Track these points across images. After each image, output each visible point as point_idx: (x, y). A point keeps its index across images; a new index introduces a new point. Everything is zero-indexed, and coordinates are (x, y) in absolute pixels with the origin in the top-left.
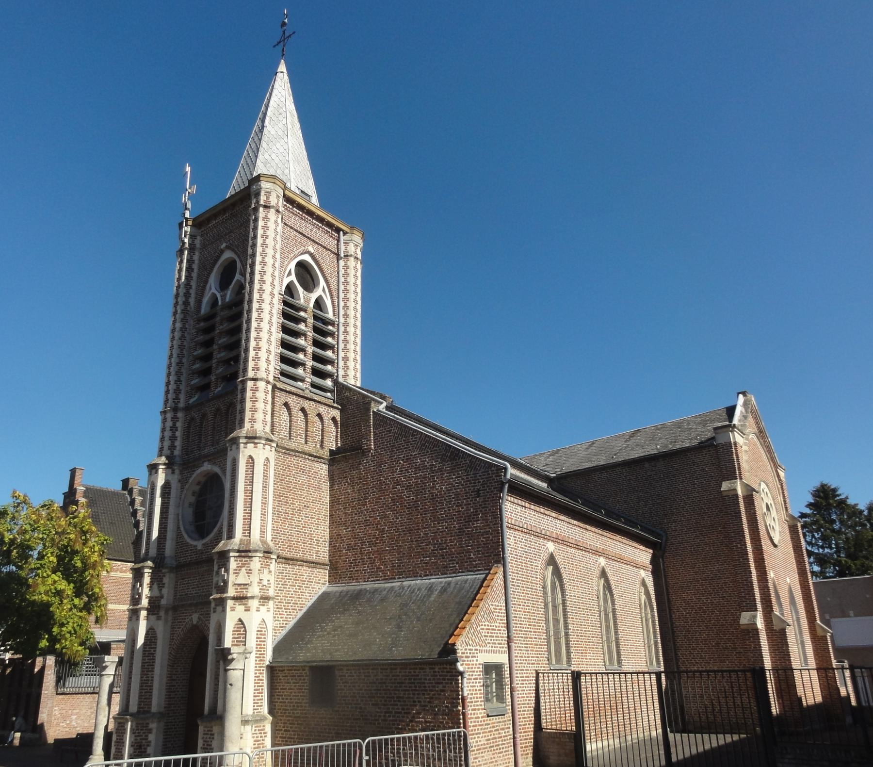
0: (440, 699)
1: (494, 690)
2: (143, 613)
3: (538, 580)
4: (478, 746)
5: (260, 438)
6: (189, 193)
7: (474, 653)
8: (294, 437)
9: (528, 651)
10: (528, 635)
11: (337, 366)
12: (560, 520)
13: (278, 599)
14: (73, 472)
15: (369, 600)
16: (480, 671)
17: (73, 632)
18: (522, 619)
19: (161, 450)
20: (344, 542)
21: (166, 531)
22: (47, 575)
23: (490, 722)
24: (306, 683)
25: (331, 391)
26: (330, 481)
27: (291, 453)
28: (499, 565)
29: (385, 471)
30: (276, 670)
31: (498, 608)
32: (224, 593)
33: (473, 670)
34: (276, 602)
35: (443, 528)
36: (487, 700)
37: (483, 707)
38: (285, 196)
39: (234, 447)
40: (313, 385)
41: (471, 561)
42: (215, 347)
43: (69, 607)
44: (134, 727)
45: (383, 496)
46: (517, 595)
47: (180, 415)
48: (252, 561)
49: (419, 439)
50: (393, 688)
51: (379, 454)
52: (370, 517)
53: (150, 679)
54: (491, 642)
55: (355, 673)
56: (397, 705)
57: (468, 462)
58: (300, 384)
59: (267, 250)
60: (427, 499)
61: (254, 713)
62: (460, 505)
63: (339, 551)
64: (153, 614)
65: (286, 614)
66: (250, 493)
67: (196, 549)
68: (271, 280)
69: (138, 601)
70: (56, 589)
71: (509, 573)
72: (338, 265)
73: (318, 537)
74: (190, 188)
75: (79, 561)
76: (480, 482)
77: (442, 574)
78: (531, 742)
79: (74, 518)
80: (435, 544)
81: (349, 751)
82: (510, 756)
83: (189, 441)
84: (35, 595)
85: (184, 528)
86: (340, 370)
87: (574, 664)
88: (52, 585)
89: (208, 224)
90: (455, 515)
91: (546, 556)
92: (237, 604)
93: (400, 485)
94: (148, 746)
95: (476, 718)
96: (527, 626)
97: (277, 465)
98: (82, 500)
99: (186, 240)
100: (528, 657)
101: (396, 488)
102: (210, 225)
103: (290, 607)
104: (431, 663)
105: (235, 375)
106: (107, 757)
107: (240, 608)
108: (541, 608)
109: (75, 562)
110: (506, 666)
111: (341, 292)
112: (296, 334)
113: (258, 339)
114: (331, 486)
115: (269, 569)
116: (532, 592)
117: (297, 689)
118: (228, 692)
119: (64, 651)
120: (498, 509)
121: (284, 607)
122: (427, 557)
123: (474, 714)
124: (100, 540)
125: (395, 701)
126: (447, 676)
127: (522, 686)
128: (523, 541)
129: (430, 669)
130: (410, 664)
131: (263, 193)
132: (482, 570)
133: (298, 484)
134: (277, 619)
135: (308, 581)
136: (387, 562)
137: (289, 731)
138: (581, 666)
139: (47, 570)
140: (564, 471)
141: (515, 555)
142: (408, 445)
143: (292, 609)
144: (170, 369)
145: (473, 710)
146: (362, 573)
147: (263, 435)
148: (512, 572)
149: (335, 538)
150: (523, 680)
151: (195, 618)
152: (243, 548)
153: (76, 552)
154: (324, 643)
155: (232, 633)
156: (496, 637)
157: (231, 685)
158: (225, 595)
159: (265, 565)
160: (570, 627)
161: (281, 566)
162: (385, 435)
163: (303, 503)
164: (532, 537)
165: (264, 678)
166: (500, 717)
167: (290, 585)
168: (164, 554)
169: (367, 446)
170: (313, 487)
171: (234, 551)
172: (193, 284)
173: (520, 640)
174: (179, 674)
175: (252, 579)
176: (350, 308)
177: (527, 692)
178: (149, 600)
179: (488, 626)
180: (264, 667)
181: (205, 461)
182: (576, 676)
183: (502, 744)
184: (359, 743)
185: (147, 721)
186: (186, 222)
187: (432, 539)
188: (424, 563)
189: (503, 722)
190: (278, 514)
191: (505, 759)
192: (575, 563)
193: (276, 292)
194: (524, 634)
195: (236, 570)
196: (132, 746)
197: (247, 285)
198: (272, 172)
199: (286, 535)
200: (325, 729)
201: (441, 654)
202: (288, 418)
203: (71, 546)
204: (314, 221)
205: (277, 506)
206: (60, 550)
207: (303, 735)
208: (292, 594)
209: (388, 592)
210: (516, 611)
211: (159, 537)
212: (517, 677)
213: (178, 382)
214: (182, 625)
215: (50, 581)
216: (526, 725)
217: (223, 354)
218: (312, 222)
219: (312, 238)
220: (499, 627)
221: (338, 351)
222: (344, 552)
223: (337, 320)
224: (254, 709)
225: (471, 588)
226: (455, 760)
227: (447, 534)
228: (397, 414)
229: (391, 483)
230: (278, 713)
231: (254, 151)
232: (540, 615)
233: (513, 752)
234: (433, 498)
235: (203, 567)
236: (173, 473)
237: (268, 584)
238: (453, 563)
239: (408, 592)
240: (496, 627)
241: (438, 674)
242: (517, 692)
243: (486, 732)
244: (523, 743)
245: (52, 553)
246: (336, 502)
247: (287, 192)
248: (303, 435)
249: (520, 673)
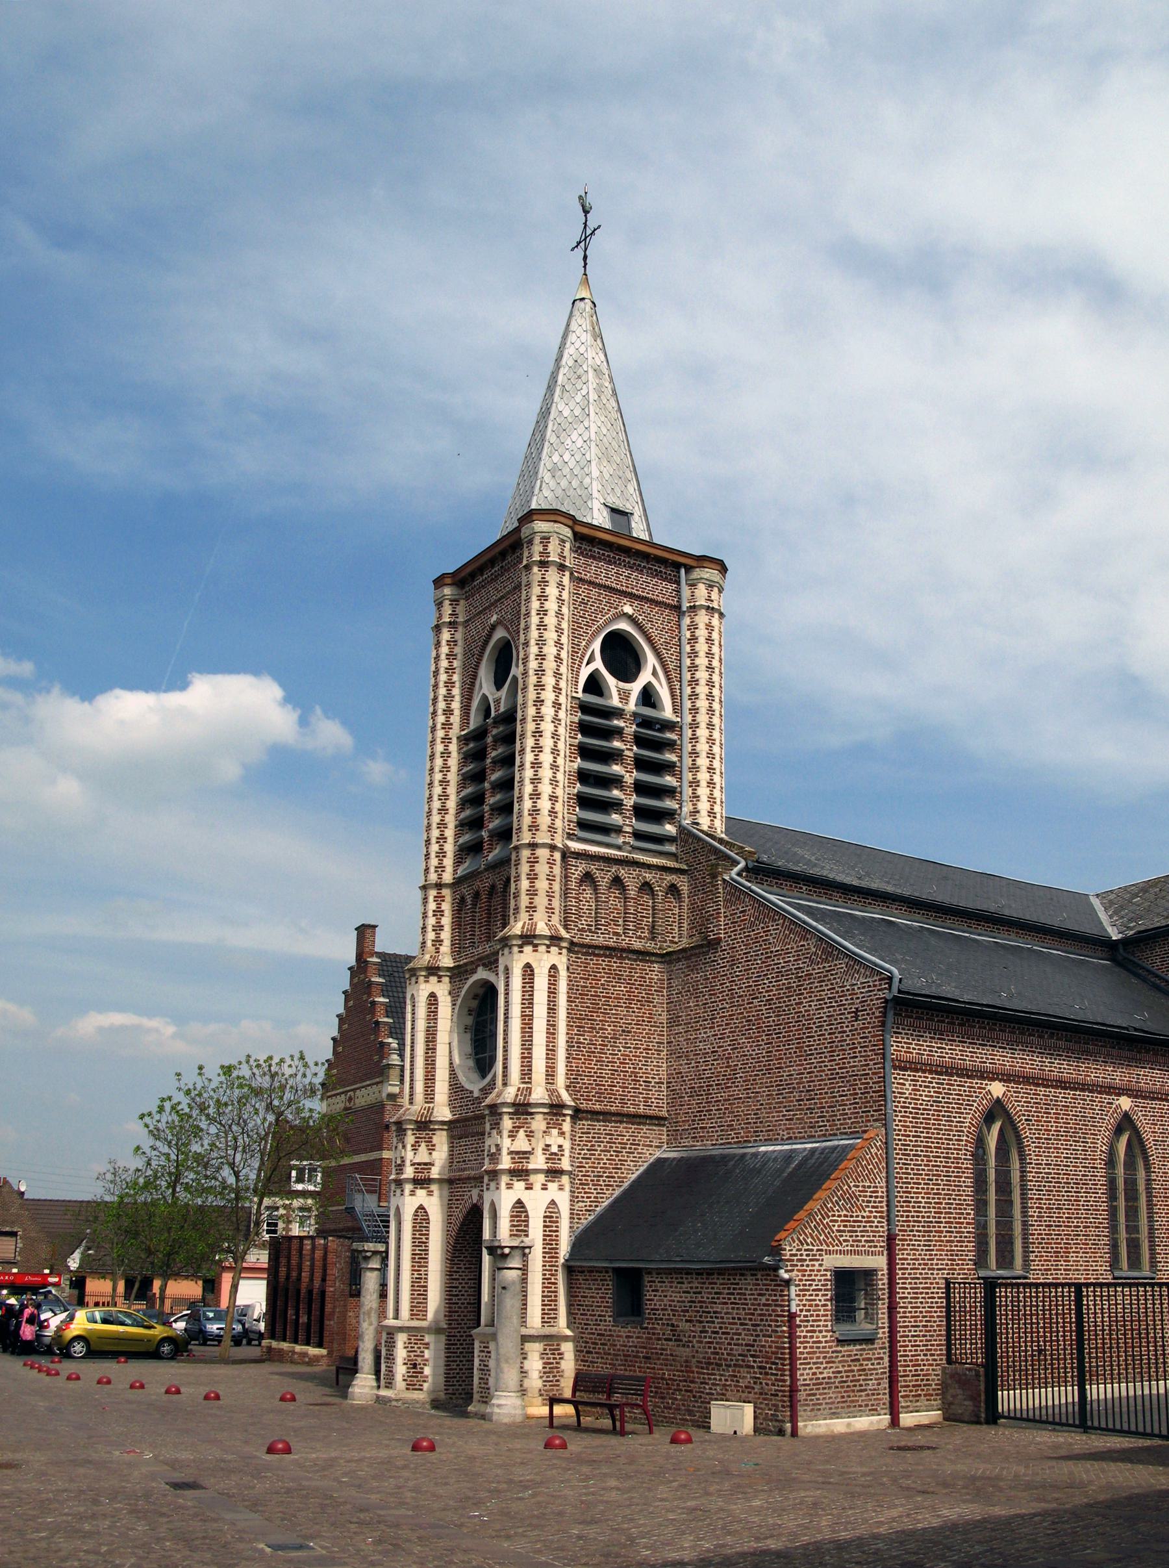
13: (581, 1171)
33: (813, 1277)
37: (830, 1328)
40: (638, 835)
47: (446, 892)
73: (647, 1077)
89: (473, 581)
103: (601, 1183)
107: (519, 1185)
115: (560, 1129)
131: (537, 540)
133: (610, 998)
137: (591, 1353)
143: (605, 1185)
159: (554, 1124)
170: (638, 1001)
181: (479, 966)
199: (593, 1076)
205: (576, 1034)
208: (605, 1164)
217: (498, 797)
247: (579, 529)
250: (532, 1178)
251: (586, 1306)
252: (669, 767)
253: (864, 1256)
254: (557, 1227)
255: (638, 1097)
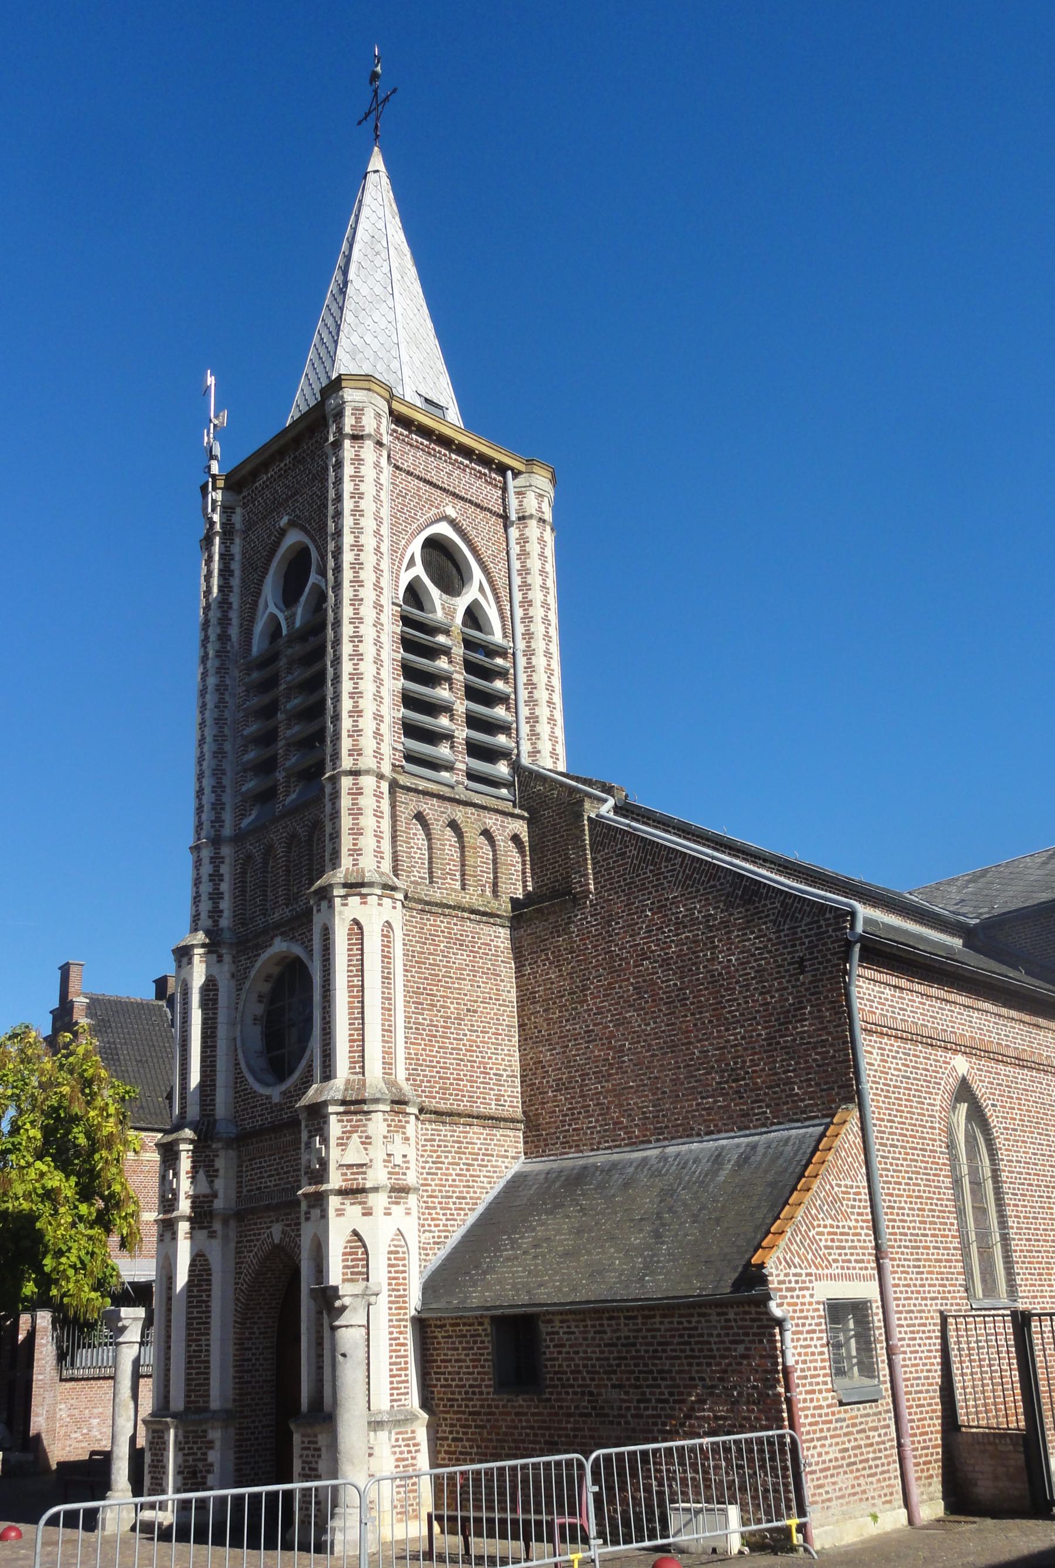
0: (740, 1372)
1: (854, 1353)
2: (184, 1227)
3: (937, 1131)
4: (824, 1462)
5: (371, 885)
6: (215, 426)
7: (804, 1282)
8: (438, 878)
9: (922, 1273)
10: (921, 1241)
11: (517, 735)
12: (978, 1010)
13: (427, 1191)
14: (65, 971)
15: (601, 1187)
16: (819, 1317)
17: (79, 1265)
18: (906, 1212)
19: (196, 918)
20: (549, 1076)
21: (215, 1071)
22: (27, 1162)
23: (847, 1416)
24: (487, 1348)
25: (509, 785)
26: (515, 958)
27: (434, 909)
28: (851, 1106)
29: (617, 934)
30: (430, 1326)
31: (852, 1191)
32: (321, 1182)
33: (805, 1314)
34: (422, 1197)
35: (736, 1039)
36: (839, 1372)
37: (830, 1386)
38: (391, 412)
39: (324, 904)
40: (472, 776)
41: (793, 1102)
42: (281, 716)
43: (69, 1219)
44: (181, 1438)
45: (616, 982)
46: (891, 1164)
47: (226, 851)
48: (370, 1120)
49: (681, 867)
50: (651, 1353)
51: (604, 902)
52: (594, 1025)
53: (204, 1348)
54: (840, 1258)
55: (577, 1327)
56: (659, 1386)
57: (777, 905)
58: (445, 775)
59: (363, 522)
60: (702, 984)
61: (392, 1406)
62: (768, 992)
63: (540, 1093)
64: (200, 1228)
65: (444, 1218)
66: (359, 992)
67: (270, 1103)
68: (374, 580)
69: (173, 1205)
70: (43, 1187)
71: (872, 1120)
72: (507, 538)
74: (216, 417)
75: (81, 1135)
76: (804, 943)
77: (740, 1129)
78: (937, 1453)
79: (66, 1057)
80: (723, 1071)
81: (559, 1477)
82: (892, 1482)
83: (245, 900)
84: (7, 1201)
85: (248, 1065)
86: (522, 742)
87: (1023, 1297)
88: (37, 1181)
89: (254, 482)
90: (758, 1012)
91: (953, 1083)
92: (347, 1202)
93: (649, 958)
94: (209, 1472)
95: (815, 1408)
96: (918, 1225)
97: (408, 935)
98: (83, 1021)
99: (216, 518)
100: (923, 1286)
101: (642, 965)
102: (257, 484)
103: (451, 1206)
104: (720, 1305)
105: (319, 768)
106: (137, 1491)
107: (353, 1211)
108: (946, 1188)
109: (75, 1138)
110: (874, 1305)
111: (515, 589)
112: (432, 679)
113: (356, 695)
114: (519, 969)
115: (404, 1133)
116: (924, 1156)
117: (472, 1361)
118: (339, 1369)
119: (66, 1300)
120: (841, 995)
121: (439, 1206)
122: (708, 1097)
123: (812, 1400)
124: (118, 1094)
125: (655, 1379)
126: (752, 1327)
127: (912, 1343)
128: (901, 1055)
129: (718, 1314)
130: (678, 1306)
131: (348, 412)
132: (816, 1117)
133: (451, 968)
134: (427, 1228)
135: (484, 1155)
136: (632, 1109)
137: (461, 1440)
138: (1040, 1300)
139: (25, 1153)
140: (996, 912)
141: (884, 1084)
142: (659, 879)
144: (201, 765)
145: (807, 1392)
146: (585, 1134)
147: (376, 878)
148: (878, 1119)
149: (531, 1070)
150: (912, 1332)
151: (277, 1231)
152: (352, 1096)
153: (75, 1119)
154: (517, 1272)
155: (341, 1258)
156: (850, 1248)
157: (344, 1355)
158: (324, 1187)
159: (396, 1126)
160: (1010, 1224)
161: (429, 1127)
162: (614, 862)
163: (465, 1005)
164: (920, 1048)
165: (408, 1342)
166: (867, 1405)
167: (449, 1163)
168: (213, 1115)
169: (581, 886)
170: (483, 973)
171: (336, 1102)
172: (235, 599)
173: (903, 1253)
174: (257, 1338)
175: (371, 1156)
176: (534, 619)
177: (923, 1355)
178: (192, 1202)
179: (832, 1226)
180: (406, 1320)
181: (276, 936)
182: (1022, 1322)
183: (874, 1459)
184: (578, 1460)
185: (204, 1427)
186: (214, 483)
187: (716, 1061)
188: (703, 1109)
189: (875, 1414)
190: (417, 1029)
191: (883, 1488)
192: (1015, 1096)
193: (385, 600)
194: (910, 1241)
195: (342, 1138)
196: (179, 1473)
197: (330, 593)
198: (366, 369)
199: (435, 1067)
200: (527, 1435)
201: (737, 1286)
202: (426, 842)
203: (65, 1108)
204: (454, 456)
205: (413, 1013)
206: (48, 1116)
207: (487, 1447)
208: (454, 1180)
209: (637, 1168)
210: (892, 1195)
211: (202, 1084)
212: (902, 1326)
213: (218, 788)
214: (255, 1246)
215: (32, 1174)
216: (925, 1419)
217: (297, 728)
218: (450, 458)
219: (451, 489)
220: (856, 1228)
221: (516, 705)
222: (550, 1094)
223: (511, 644)
224: (392, 1401)
225: (796, 1154)
226: (776, 1491)
227: (745, 1049)
228: (638, 821)
229: (632, 957)
230: (438, 1406)
231: (330, 333)
232: (944, 1203)
233: (898, 1473)
234: (714, 979)
235: (285, 1136)
236: (220, 960)
237: (405, 1162)
238: (760, 1107)
239: (674, 1167)
240: (850, 1228)
241: (733, 1324)
242: (901, 1356)
243: (839, 1436)
244: (921, 1456)
245: (31, 1123)
246: (528, 999)
247: (395, 405)
248: (458, 874)
249: (906, 1319)
250: (372, 1199)
251: (450, 1373)
252: (501, 699)
253: (856, 1283)
254: (404, 1266)
255: (489, 1094)
